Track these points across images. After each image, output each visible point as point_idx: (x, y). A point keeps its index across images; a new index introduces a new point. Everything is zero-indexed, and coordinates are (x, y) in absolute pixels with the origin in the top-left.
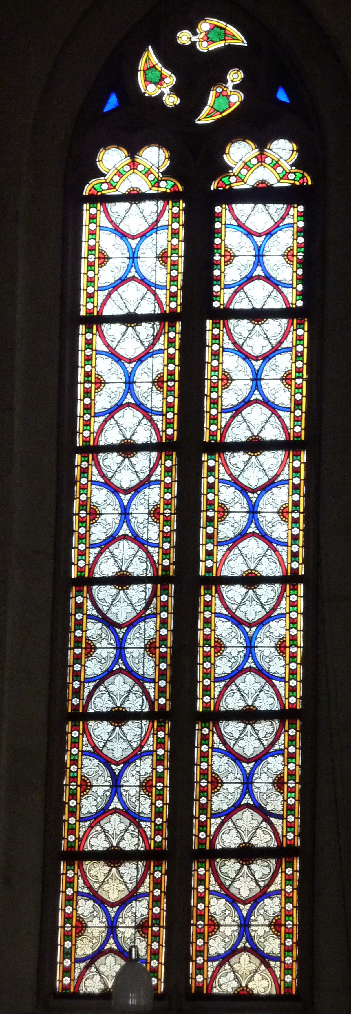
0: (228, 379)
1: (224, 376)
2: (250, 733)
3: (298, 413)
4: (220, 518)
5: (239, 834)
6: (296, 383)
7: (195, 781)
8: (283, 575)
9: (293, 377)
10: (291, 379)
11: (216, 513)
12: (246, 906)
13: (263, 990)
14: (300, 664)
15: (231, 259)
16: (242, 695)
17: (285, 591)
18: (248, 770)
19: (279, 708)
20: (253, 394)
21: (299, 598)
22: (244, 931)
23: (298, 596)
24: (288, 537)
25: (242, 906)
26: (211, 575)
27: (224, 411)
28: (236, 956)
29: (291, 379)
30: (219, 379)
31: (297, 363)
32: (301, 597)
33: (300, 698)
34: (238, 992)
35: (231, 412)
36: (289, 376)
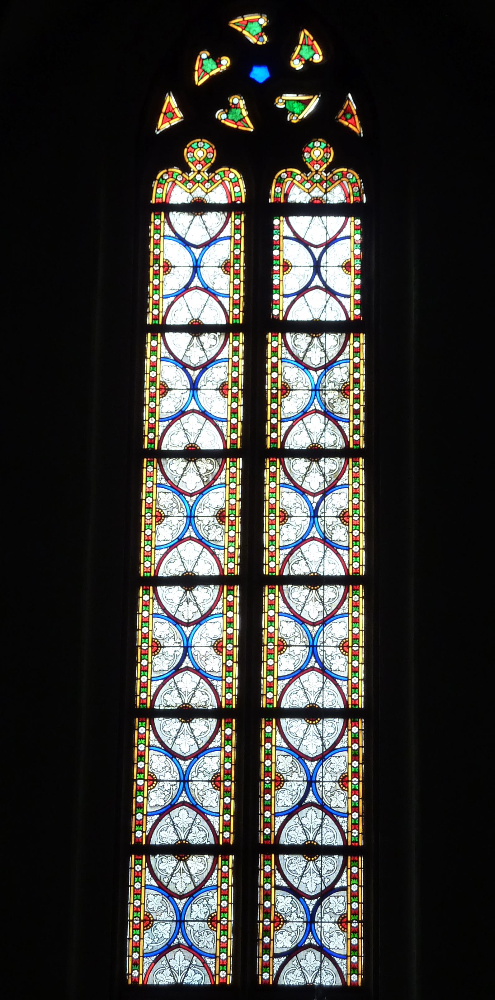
0: (153, 780)
1: (150, 777)
2: (183, 869)
3: (227, 817)
4: (161, 395)
5: (176, 832)
6: (224, 786)
7: (128, 937)
8: (228, 203)
9: (222, 779)
10: (220, 781)
11: (146, 782)
12: (192, 498)
13: (201, 840)
14: (233, 833)
15: (165, 392)
16: (175, 829)
17: (217, 862)
18: (185, 768)
19: (216, 707)
20: (180, 796)
21: (235, 598)
22: (180, 926)
23: (234, 597)
24: (223, 605)
25: (179, 900)
26: (157, 322)
27: (146, 955)
28: (172, 952)
29: (220, 781)
30: (149, 646)
31: (225, 799)
32: (236, 630)
33: (240, 500)
34: (192, 323)
35: (168, 420)
36: (228, 264)
